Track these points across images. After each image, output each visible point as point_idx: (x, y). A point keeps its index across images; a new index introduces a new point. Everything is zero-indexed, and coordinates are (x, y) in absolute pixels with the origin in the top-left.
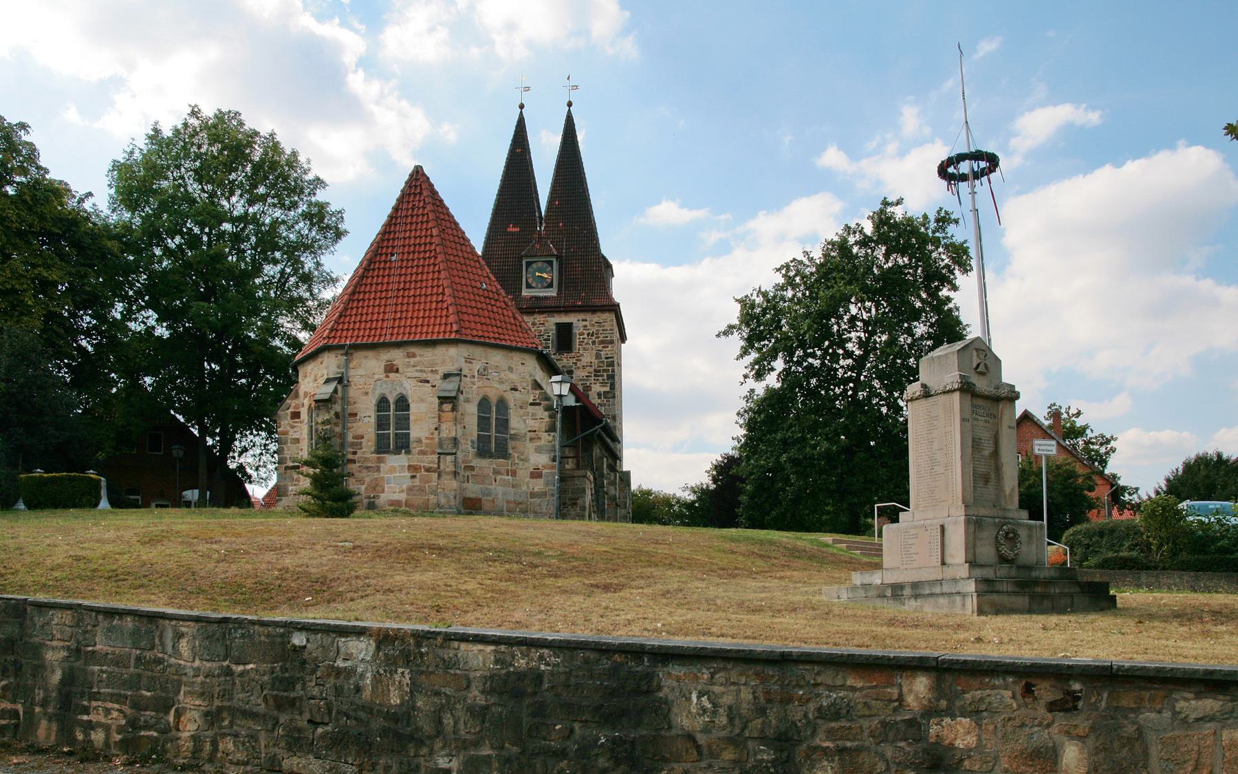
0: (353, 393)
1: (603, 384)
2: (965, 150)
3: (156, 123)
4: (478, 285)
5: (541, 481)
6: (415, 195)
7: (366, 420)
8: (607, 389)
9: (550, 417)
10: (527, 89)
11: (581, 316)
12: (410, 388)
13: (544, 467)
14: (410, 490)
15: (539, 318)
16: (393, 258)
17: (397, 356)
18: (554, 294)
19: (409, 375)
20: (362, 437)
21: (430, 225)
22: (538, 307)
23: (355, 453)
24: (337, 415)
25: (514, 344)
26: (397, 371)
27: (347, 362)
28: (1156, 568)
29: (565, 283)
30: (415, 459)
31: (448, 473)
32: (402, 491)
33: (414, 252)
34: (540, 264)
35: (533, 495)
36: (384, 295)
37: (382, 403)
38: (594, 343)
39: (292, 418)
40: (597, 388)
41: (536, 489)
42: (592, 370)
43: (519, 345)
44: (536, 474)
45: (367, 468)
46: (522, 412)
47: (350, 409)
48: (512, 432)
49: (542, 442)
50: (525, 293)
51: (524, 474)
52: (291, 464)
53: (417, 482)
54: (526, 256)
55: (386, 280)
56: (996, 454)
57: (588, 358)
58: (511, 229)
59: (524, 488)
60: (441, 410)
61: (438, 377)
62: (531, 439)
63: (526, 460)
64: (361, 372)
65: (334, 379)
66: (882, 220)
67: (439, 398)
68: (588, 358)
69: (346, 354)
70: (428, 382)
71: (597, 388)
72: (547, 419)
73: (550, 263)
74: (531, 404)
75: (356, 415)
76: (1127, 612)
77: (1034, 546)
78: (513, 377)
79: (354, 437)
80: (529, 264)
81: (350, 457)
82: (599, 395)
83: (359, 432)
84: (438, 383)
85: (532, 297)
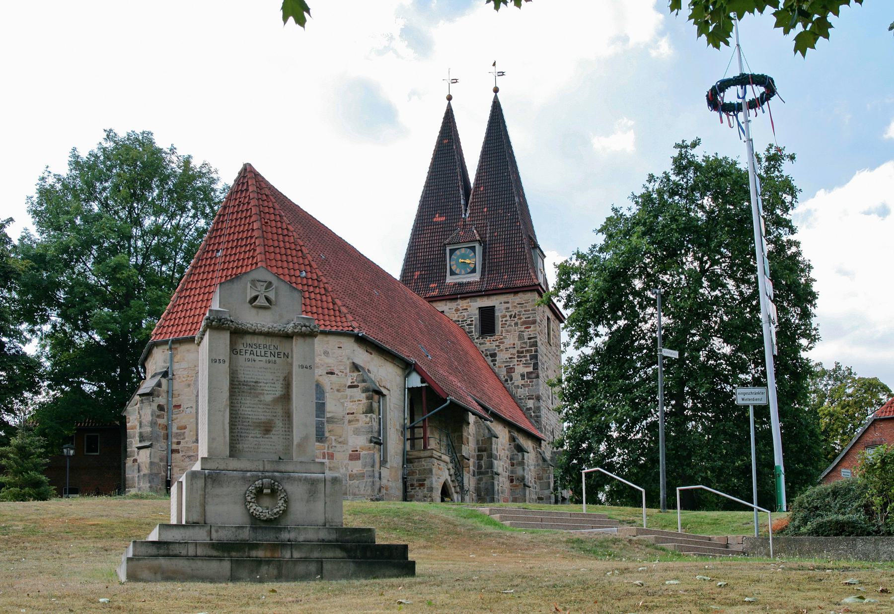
0: (177, 385)
1: (526, 365)
2: (730, 76)
3: (74, 149)
4: (297, 273)
5: (359, 463)
6: (242, 191)
8: (531, 369)
9: (368, 398)
10: (455, 81)
11: (503, 298)
15: (462, 304)
16: (219, 254)
18: (478, 279)
20: (185, 428)
21: (253, 219)
23: (178, 443)
24: (161, 408)
27: (172, 357)
28: (877, 532)
29: (488, 266)
34: (463, 251)
36: (207, 290)
38: (516, 324)
40: (520, 369)
41: (355, 472)
42: (515, 351)
43: (334, 329)
45: (189, 457)
47: (175, 401)
48: (328, 415)
49: (359, 424)
50: (450, 280)
51: (341, 456)
54: (449, 244)
56: (286, 397)
57: (511, 339)
58: (438, 219)
62: (350, 422)
64: (184, 365)
65: (159, 373)
66: (682, 164)
68: (511, 339)
72: (365, 401)
73: (473, 249)
74: (350, 387)
75: (179, 406)
76: (434, 580)
77: (320, 506)
79: (180, 428)
80: (452, 251)
81: (175, 447)
82: (523, 376)
83: (182, 424)
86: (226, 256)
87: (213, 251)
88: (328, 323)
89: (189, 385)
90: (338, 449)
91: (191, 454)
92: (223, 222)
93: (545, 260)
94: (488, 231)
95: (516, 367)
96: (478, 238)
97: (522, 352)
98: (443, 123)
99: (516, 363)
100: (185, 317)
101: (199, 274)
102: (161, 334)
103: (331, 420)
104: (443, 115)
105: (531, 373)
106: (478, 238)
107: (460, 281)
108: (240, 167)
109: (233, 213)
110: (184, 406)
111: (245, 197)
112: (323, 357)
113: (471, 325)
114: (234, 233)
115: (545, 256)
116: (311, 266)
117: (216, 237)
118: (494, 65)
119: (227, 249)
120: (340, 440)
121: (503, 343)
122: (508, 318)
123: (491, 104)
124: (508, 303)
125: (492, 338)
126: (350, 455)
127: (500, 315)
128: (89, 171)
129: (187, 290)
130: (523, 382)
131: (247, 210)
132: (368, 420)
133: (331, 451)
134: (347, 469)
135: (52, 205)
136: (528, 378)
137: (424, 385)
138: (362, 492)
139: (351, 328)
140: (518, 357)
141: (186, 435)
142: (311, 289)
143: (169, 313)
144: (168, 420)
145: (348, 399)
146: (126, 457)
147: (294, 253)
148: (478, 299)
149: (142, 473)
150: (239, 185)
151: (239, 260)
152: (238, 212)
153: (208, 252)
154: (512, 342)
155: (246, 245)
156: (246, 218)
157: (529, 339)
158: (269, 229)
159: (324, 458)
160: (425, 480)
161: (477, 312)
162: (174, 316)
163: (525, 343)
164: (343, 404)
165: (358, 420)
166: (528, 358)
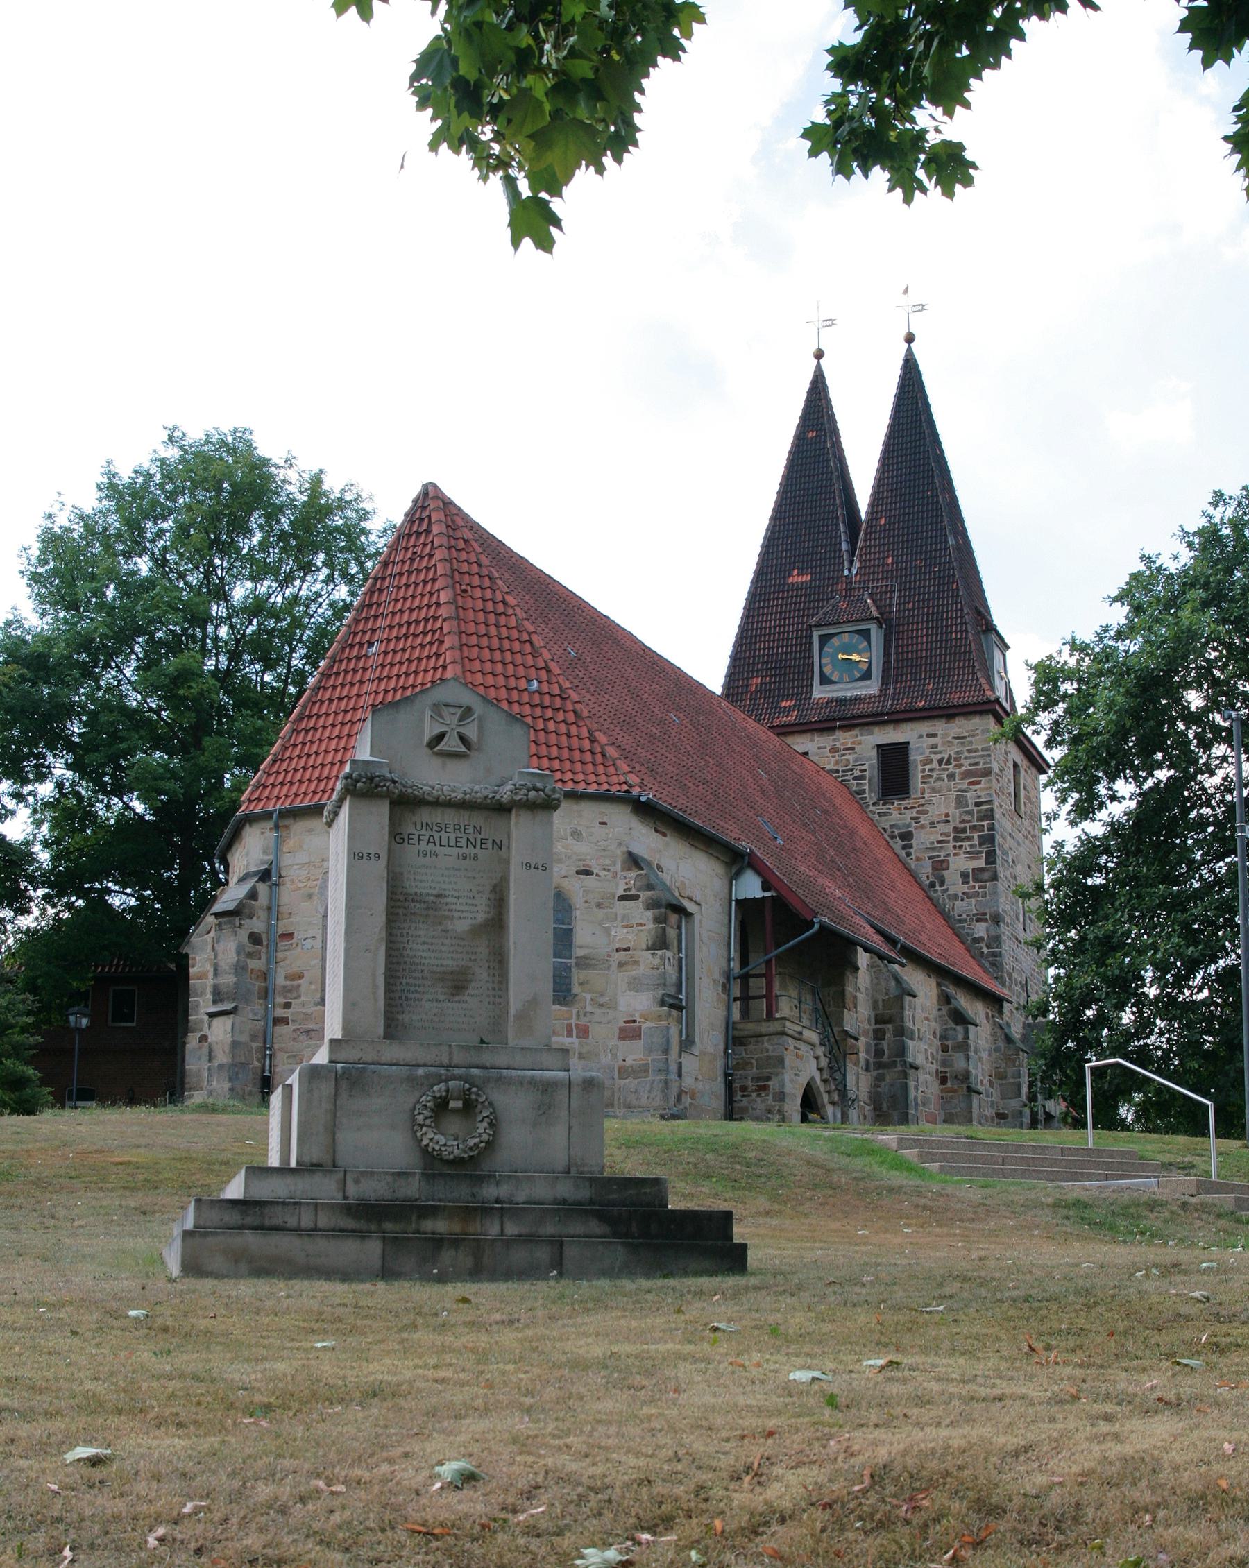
0: (287, 896)
1: (972, 854)
4: (523, 684)
6: (419, 534)
7: (309, 943)
8: (981, 863)
9: (657, 920)
11: (925, 727)
13: (646, 1017)
15: (844, 738)
16: (373, 650)
18: (874, 691)
20: (300, 976)
22: (843, 718)
23: (287, 1006)
25: (580, 788)
27: (279, 842)
29: (896, 666)
33: (406, 636)
34: (846, 638)
35: (624, 1072)
36: (348, 717)
38: (951, 776)
40: (960, 863)
41: (629, 1062)
42: (948, 828)
43: (592, 789)
44: (630, 1032)
45: (308, 1032)
46: (600, 913)
47: (283, 926)
48: (579, 953)
50: (820, 693)
51: (604, 1033)
54: (818, 625)
55: (355, 691)
56: (496, 924)
58: (796, 579)
59: (606, 1059)
63: (611, 1005)
64: (302, 857)
65: (254, 874)
69: (277, 827)
71: (960, 863)
72: (651, 925)
73: (866, 634)
75: (291, 935)
76: (786, 1282)
78: (583, 848)
80: (824, 640)
81: (280, 1012)
82: (965, 876)
83: (295, 969)
85: (831, 701)
86: (386, 653)
89: (310, 896)
93: (1008, 653)
96: (875, 614)
97: (964, 830)
98: (807, 400)
99: (952, 851)
101: (334, 687)
104: (807, 387)
105: (982, 870)
106: (875, 614)
107: (840, 694)
108: (415, 490)
109: (401, 574)
110: (299, 936)
111: (425, 545)
112: (570, 841)
114: (402, 611)
115: (1007, 647)
117: (367, 619)
118: (906, 291)
120: (601, 1000)
121: (926, 812)
122: (935, 765)
123: (900, 363)
124: (935, 735)
125: (905, 803)
126: (622, 1030)
127: (919, 758)
129: (310, 717)
130: (965, 888)
131: (428, 569)
132: (657, 961)
134: (614, 1056)
136: (976, 880)
137: (768, 894)
138: (644, 1101)
140: (956, 839)
141: (302, 990)
142: (549, 713)
146: (186, 1031)
148: (876, 729)
149: (216, 1063)
150: (412, 522)
152: (410, 573)
153: (352, 646)
154: (943, 811)
157: (977, 804)
158: (470, 603)
159: (569, 1034)
160: (769, 1079)
161: (874, 753)
162: (284, 766)
163: (970, 813)
164: (607, 930)
165: (636, 963)
166: (976, 842)
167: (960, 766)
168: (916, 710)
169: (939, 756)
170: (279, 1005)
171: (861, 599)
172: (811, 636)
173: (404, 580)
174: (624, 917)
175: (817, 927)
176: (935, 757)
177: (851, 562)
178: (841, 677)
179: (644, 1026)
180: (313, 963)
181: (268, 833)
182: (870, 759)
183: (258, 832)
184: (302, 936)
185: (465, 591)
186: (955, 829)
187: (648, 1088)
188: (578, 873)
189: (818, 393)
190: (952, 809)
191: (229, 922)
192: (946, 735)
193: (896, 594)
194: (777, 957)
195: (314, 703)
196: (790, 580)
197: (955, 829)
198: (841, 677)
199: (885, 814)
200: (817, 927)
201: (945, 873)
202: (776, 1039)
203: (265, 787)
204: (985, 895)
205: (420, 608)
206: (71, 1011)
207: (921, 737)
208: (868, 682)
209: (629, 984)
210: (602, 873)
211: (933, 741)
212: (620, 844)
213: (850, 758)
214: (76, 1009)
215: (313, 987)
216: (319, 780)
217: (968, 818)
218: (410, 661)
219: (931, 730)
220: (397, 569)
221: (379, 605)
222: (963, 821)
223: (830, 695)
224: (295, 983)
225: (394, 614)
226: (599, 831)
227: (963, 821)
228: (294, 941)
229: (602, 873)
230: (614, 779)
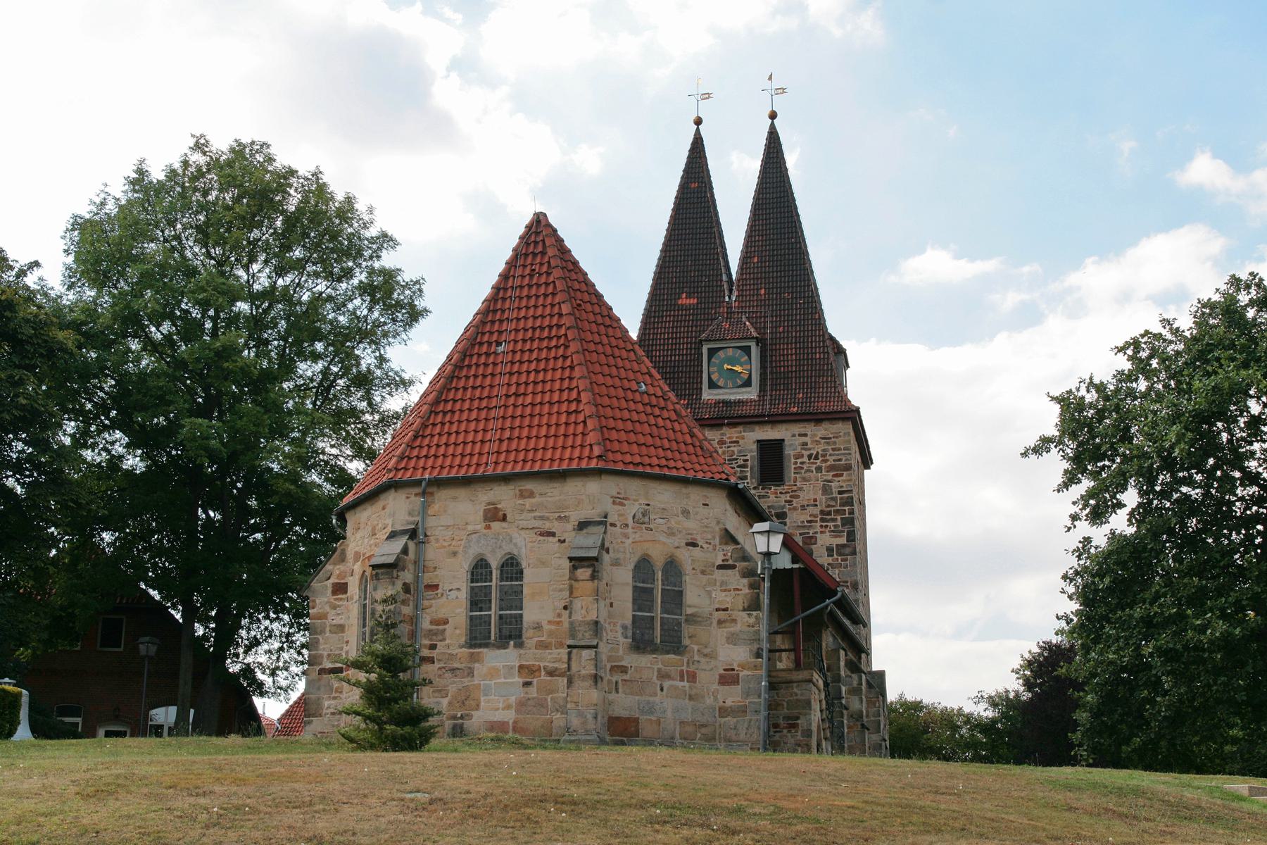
1: (836, 533)
3: (142, 161)
5: (738, 689)
6: (535, 255)
7: (453, 594)
8: (843, 540)
9: (751, 586)
10: (707, 96)
11: (797, 428)
12: (523, 545)
13: (743, 667)
14: (521, 704)
15: (730, 433)
16: (500, 349)
17: (503, 495)
19: (523, 524)
20: (446, 622)
24: (407, 589)
25: (691, 475)
26: (504, 518)
29: (771, 377)
30: (530, 655)
31: (584, 678)
32: (508, 707)
34: (730, 352)
35: (723, 712)
36: (484, 403)
37: (480, 569)
38: (819, 469)
39: (334, 592)
40: (825, 540)
41: (729, 703)
42: (817, 511)
43: (700, 476)
44: (728, 678)
45: (453, 670)
46: (705, 579)
47: (427, 579)
48: (689, 611)
49: (738, 628)
50: (707, 395)
51: (708, 678)
52: (328, 665)
53: (533, 692)
57: (811, 492)
58: (684, 301)
59: (709, 701)
60: (573, 578)
61: (569, 527)
62: (720, 622)
63: (711, 656)
64: (445, 520)
65: (403, 532)
67: (571, 559)
69: (424, 494)
70: (553, 534)
71: (825, 540)
73: (747, 350)
74: (720, 567)
75: (436, 587)
78: (691, 524)
80: (712, 352)
81: (426, 653)
82: (830, 550)
83: (442, 614)
84: (570, 536)
86: (514, 352)
87: (490, 344)
88: (688, 466)
89: (455, 554)
90: (703, 666)
91: (456, 665)
92: (504, 299)
94: (769, 325)
95: (818, 536)
96: (755, 334)
97: (829, 513)
98: (689, 157)
99: (819, 529)
100: (447, 445)
101: (467, 377)
102: (406, 469)
103: (692, 619)
104: (689, 147)
105: (843, 546)
106: (755, 334)
107: (726, 397)
108: (528, 219)
109: (521, 287)
110: (445, 586)
111: (541, 264)
112: (681, 518)
113: (744, 466)
114: (526, 318)
116: (651, 376)
117: (493, 322)
118: (770, 78)
119: (516, 342)
120: (706, 651)
121: (798, 497)
122: (805, 459)
123: (766, 135)
124: (805, 435)
125: (780, 489)
126: (721, 676)
127: (792, 453)
128: (152, 199)
129: (446, 401)
130: (830, 560)
131: (547, 284)
132: (752, 620)
133: (692, 668)
134: (716, 698)
135: (102, 246)
136: (839, 554)
138: (742, 736)
139: (724, 476)
140: (822, 520)
141: (447, 633)
142: (657, 412)
143: (416, 437)
144: (416, 607)
145: (718, 587)
147: (624, 354)
148: (757, 428)
150: (528, 244)
151: (538, 360)
152: (530, 286)
153: (481, 344)
154: (813, 497)
155: (550, 338)
156: (546, 296)
157: (840, 493)
158: (584, 316)
160: (798, 718)
161: (754, 447)
162: (426, 441)
163: (834, 499)
164: (709, 593)
165: (734, 621)
167: (826, 461)
168: (792, 414)
169: (808, 453)
170: (425, 646)
171: (739, 321)
172: (700, 348)
173: (525, 292)
174: (723, 583)
175: (839, 595)
176: (806, 453)
177: (731, 291)
178: (726, 383)
179: (741, 674)
180: (458, 611)
181: (413, 498)
182: (751, 451)
183: (404, 496)
184: (447, 587)
185: (579, 305)
186: (822, 512)
187: (746, 725)
188: (688, 544)
189: (698, 148)
190: (819, 496)
191: (387, 573)
192: (815, 435)
193: (769, 319)
194: (664, 611)
195: (449, 390)
196: (680, 302)
197: (822, 512)
198: (726, 383)
199: (764, 497)
200: (839, 595)
201: (813, 547)
202: (804, 685)
203: (410, 458)
204: (846, 567)
205: (543, 316)
206: (142, 640)
207: (794, 436)
208: (749, 389)
209: (728, 638)
210: (705, 546)
211: (804, 439)
212: (718, 523)
213: (735, 449)
214: (147, 639)
215: (458, 631)
216: (463, 455)
217: (832, 503)
218: (538, 360)
219: (802, 431)
220: (518, 282)
221: (503, 311)
222: (829, 506)
223: (717, 397)
224: (441, 627)
225: (518, 319)
226: (703, 511)
227: (829, 506)
228: (440, 591)
229: (705, 546)
230: (714, 469)
